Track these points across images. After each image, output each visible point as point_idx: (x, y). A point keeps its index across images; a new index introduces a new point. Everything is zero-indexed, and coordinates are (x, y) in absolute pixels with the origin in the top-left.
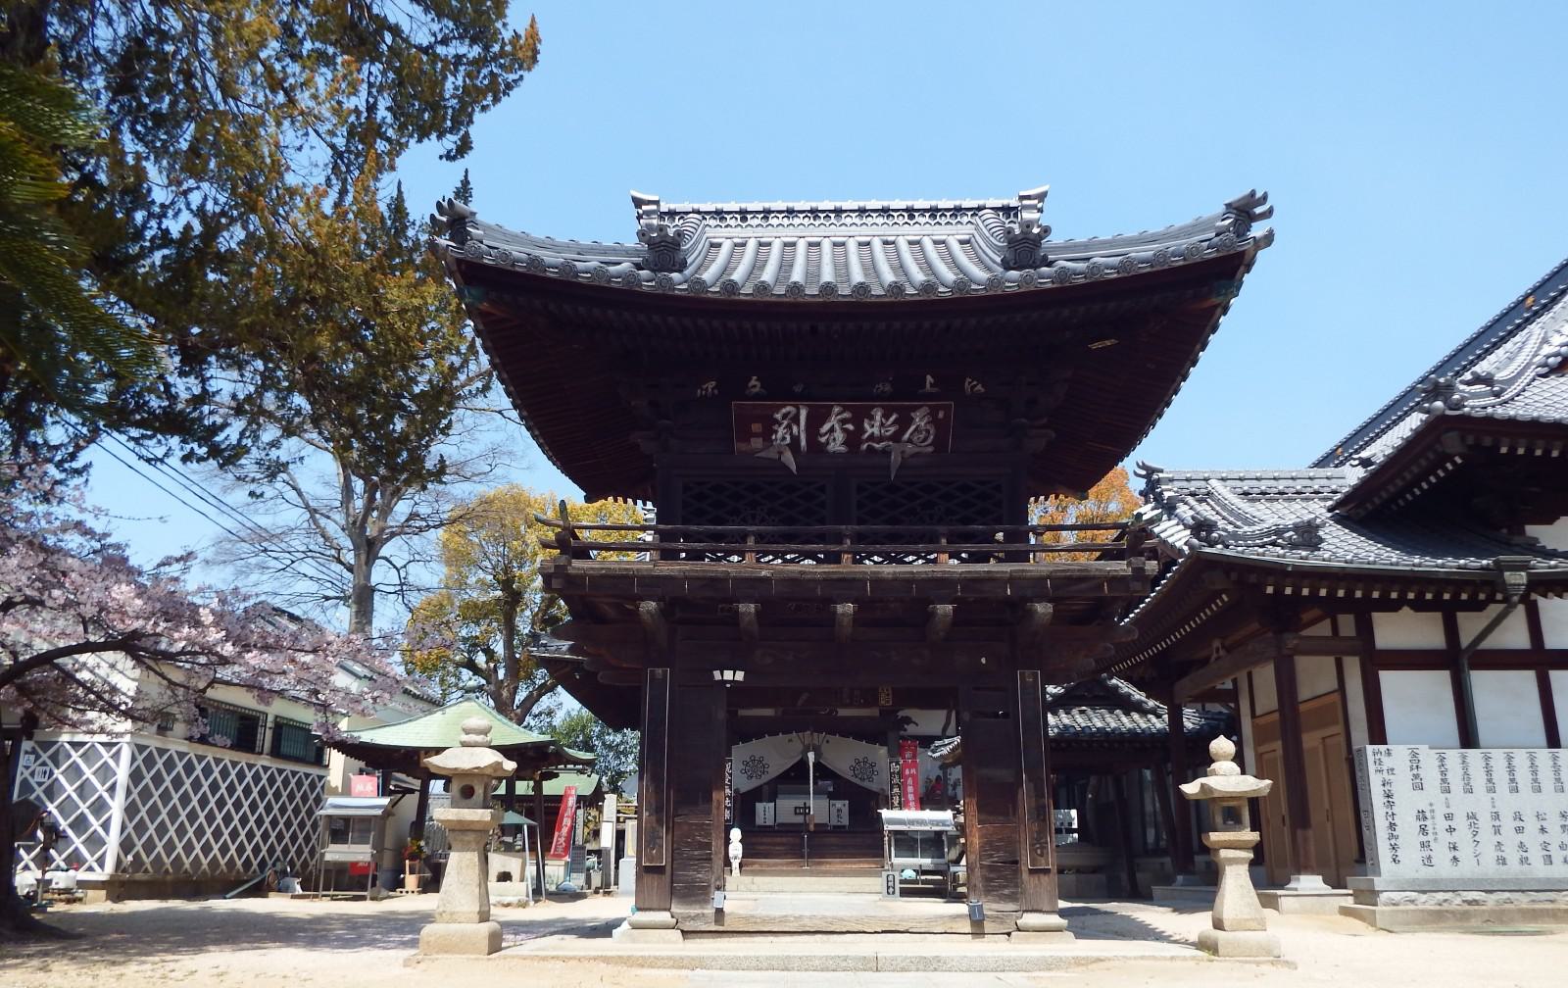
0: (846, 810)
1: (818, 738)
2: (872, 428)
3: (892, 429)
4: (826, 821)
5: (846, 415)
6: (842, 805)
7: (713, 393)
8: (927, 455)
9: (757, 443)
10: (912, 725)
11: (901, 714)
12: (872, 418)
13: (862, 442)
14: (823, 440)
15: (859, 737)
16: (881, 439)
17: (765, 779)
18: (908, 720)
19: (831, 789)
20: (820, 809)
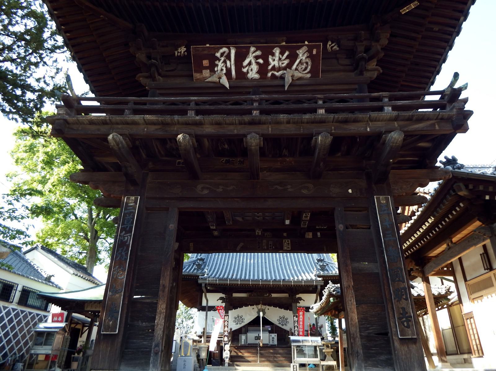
0: (276, 338)
1: (263, 307)
2: (274, 62)
3: (286, 62)
4: (268, 343)
5: (259, 53)
6: (275, 336)
7: (184, 55)
8: (306, 79)
9: (206, 73)
10: (302, 301)
11: (297, 296)
12: (273, 55)
13: (267, 71)
14: (245, 70)
15: (281, 307)
16: (279, 69)
17: (243, 324)
18: (300, 299)
19: (270, 329)
20: (265, 337)
